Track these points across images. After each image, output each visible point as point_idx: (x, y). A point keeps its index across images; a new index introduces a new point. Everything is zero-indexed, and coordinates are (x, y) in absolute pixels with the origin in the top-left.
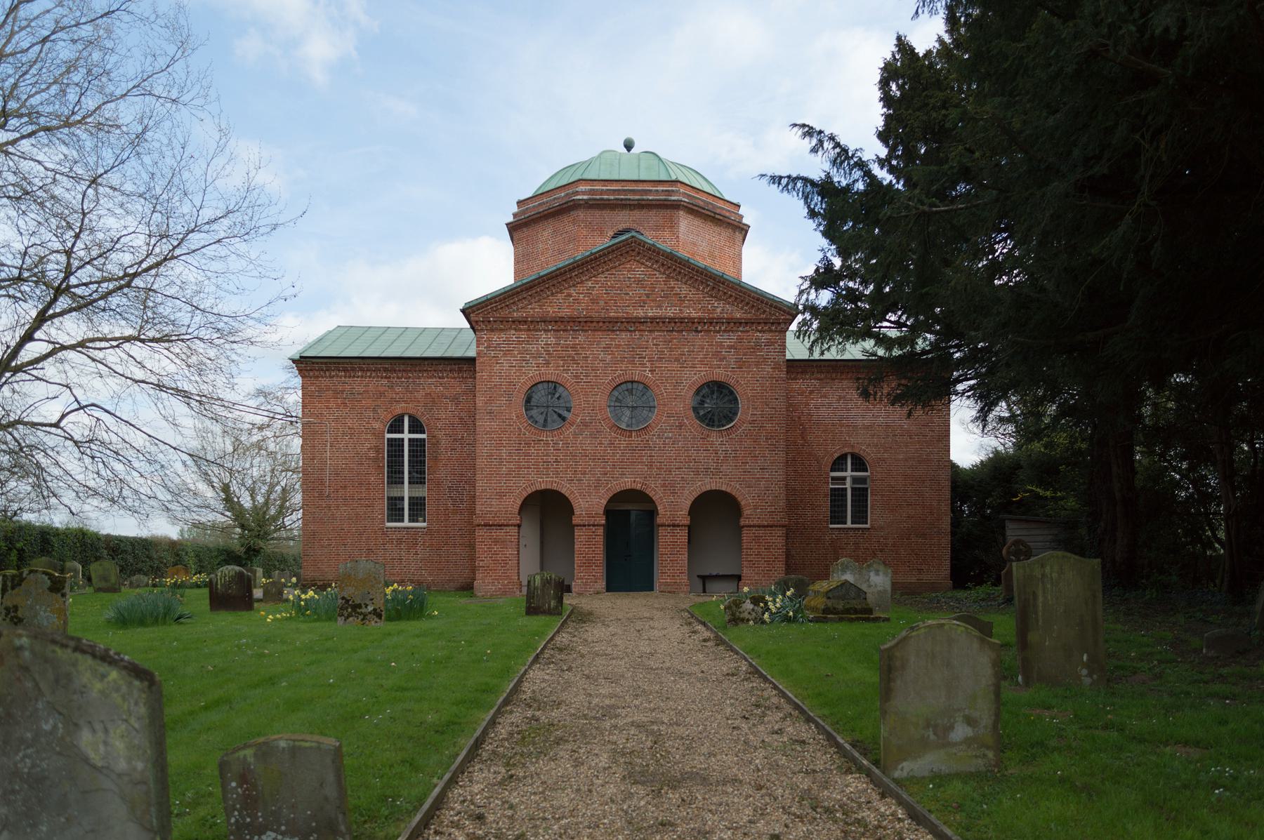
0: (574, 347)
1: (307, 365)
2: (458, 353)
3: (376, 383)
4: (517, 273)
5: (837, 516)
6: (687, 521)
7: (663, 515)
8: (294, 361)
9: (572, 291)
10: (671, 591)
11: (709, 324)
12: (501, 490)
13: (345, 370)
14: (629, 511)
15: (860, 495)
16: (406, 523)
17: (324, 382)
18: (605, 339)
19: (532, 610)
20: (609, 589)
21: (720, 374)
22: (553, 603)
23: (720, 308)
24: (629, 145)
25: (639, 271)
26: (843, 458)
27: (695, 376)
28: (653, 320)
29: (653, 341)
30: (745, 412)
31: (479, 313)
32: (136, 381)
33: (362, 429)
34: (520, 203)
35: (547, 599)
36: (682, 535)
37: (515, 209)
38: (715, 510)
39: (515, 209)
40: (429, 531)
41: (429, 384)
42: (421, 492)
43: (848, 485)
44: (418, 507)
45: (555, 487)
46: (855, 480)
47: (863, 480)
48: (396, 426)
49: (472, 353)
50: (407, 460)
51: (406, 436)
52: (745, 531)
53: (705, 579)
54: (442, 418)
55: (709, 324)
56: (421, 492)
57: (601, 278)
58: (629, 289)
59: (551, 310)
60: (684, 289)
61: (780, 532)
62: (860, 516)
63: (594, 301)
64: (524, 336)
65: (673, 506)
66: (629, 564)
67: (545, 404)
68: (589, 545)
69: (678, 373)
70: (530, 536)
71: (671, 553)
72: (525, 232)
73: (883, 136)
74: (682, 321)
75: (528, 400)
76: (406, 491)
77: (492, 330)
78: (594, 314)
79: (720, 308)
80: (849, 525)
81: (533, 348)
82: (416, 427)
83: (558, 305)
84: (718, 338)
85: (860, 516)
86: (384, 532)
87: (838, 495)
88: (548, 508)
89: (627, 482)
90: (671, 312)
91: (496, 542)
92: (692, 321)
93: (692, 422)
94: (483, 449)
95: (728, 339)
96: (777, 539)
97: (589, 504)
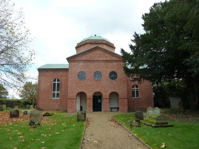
0: (87, 65)
1: (40, 70)
2: (66, 68)
3: (52, 73)
4: (77, 53)
5: (134, 96)
6: (108, 98)
7: (104, 96)
8: (37, 69)
9: (87, 55)
10: (106, 111)
11: (112, 61)
12: (73, 91)
13: (46, 71)
14: (97, 96)
15: (137, 92)
16: (56, 98)
17: (43, 73)
18: (92, 64)
19: (79, 120)
20: (94, 111)
21: (114, 70)
22: (83, 118)
23: (114, 58)
24: (95, 35)
25: (99, 52)
26: (134, 85)
27: (110, 70)
28: (101, 60)
29: (102, 64)
30: (119, 76)
31: (69, 59)
32: (147, 125)
33: (49, 82)
34: (77, 44)
35: (82, 118)
36: (108, 100)
37: (77, 45)
38: (114, 95)
39: (77, 45)
40: (60, 99)
41: (60, 73)
42: (59, 92)
43: (135, 90)
44: (58, 95)
45: (83, 91)
46: (136, 89)
47: (138, 89)
48: (55, 81)
49: (67, 67)
50: (57, 86)
51: (56, 82)
52: (120, 100)
53: (111, 108)
54: (63, 79)
55: (112, 61)
56: (59, 92)
57: (92, 53)
58: (97, 55)
59: (83, 59)
60: (107, 55)
61: (127, 99)
62: (137, 96)
63: (91, 57)
64: (78, 63)
65: (106, 94)
66: (97, 107)
67: (81, 76)
68: (90, 103)
69: (106, 70)
70: (78, 100)
71: (105, 104)
72: (78, 48)
73: (121, 53)
74: (107, 60)
75: (78, 75)
76: (56, 92)
77: (72, 62)
78: (91, 59)
79: (114, 58)
80: (136, 97)
81: (79, 65)
82: (58, 81)
83: (84, 58)
84: (114, 64)
85: (137, 96)
86: (52, 100)
87: (133, 92)
88: (82, 95)
89: (97, 90)
90: (105, 59)
91: (72, 102)
92: (109, 60)
93: (109, 78)
94: (70, 84)
95: (115, 64)
96: (126, 101)
97: (90, 95)
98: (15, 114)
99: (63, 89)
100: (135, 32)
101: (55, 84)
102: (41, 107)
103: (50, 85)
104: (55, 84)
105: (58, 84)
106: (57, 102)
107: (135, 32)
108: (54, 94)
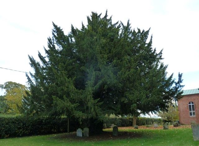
15: (190, 110)
16: (193, 116)
28: (28, 77)
41: (194, 97)
42: (194, 111)
44: (194, 113)
48: (190, 103)
51: (191, 104)
56: (194, 111)
82: (192, 103)
98: (176, 125)
99: (197, 109)
100: (72, 25)
101: (190, 106)
102: (183, 123)
103: (187, 107)
104: (190, 106)
105: (193, 106)
106: (194, 119)
107: (72, 25)
108: (191, 114)
